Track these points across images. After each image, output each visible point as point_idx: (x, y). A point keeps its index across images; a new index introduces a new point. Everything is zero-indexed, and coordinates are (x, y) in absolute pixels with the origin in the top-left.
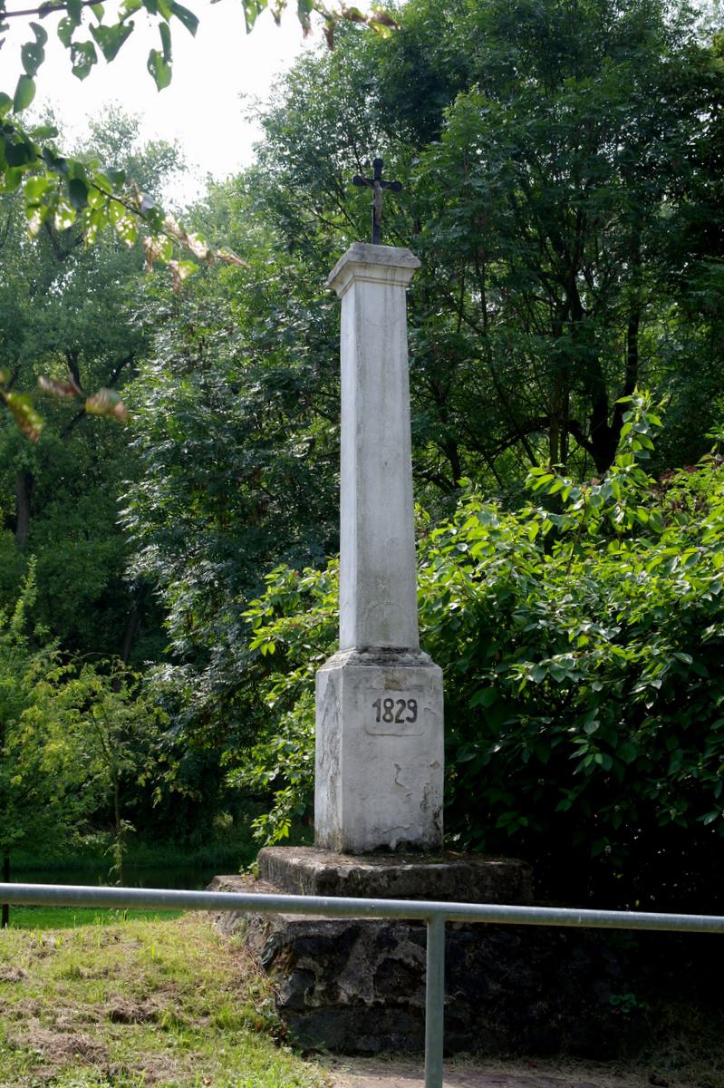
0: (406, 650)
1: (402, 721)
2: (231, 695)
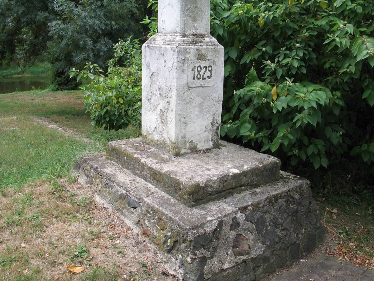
1: (205, 79)
2: (249, 231)
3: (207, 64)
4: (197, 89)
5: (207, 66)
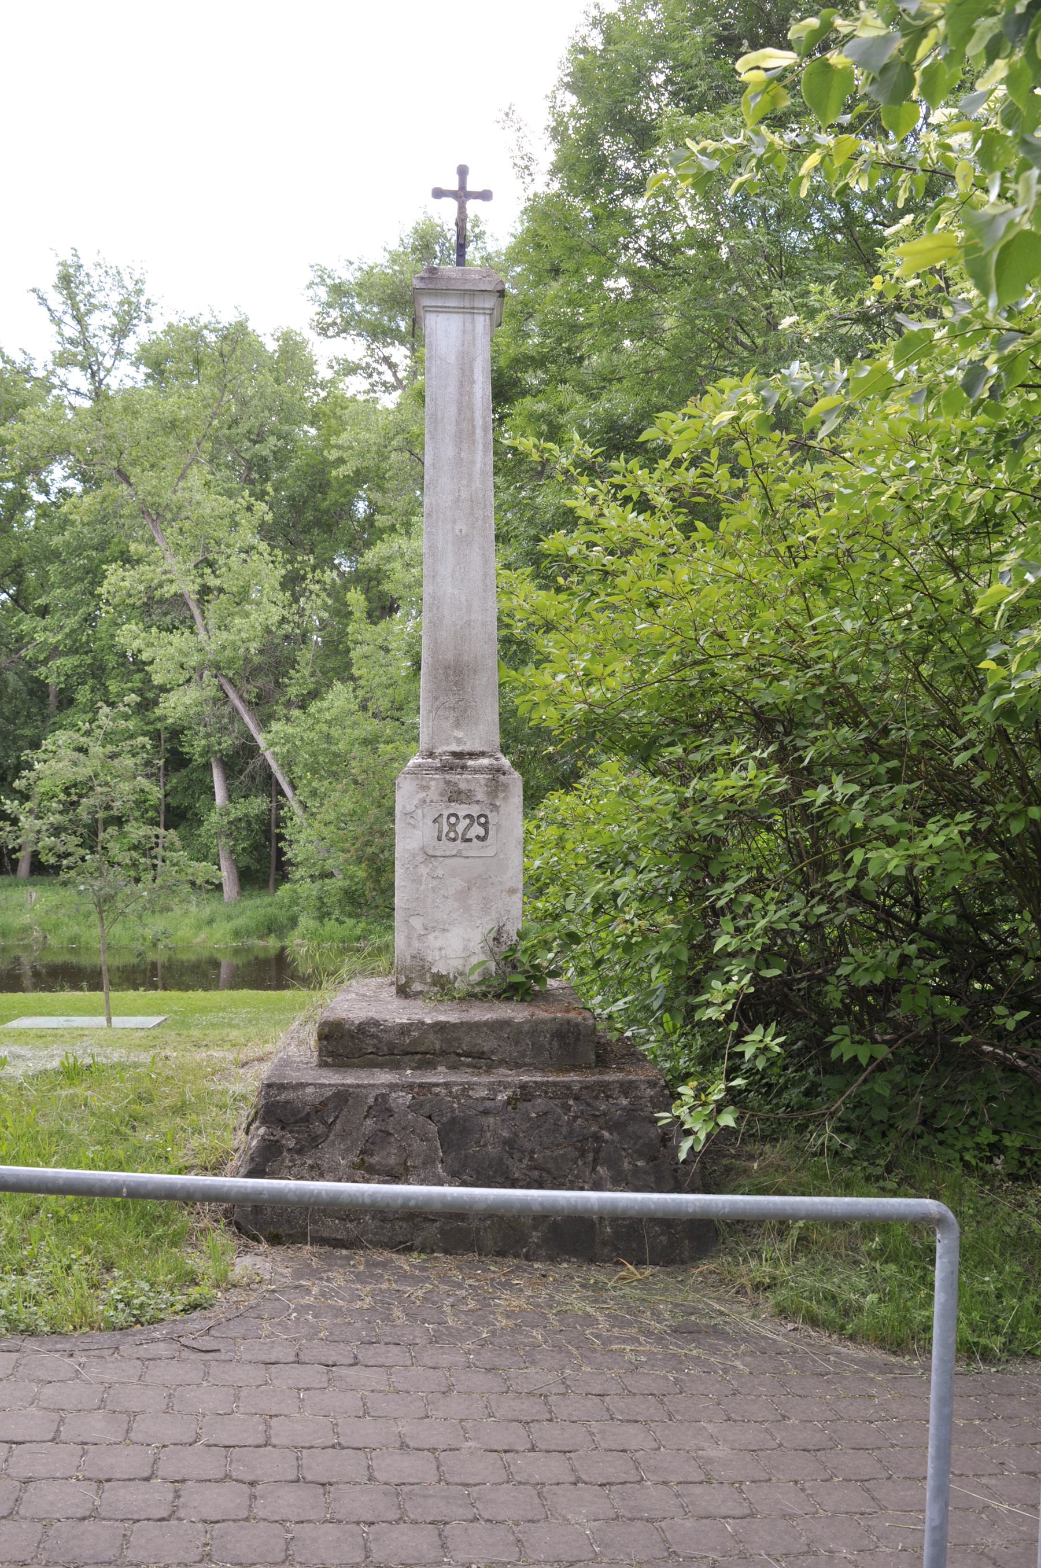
0: (483, 754)
1: (470, 840)
3: (475, 810)
4: (448, 861)
5: (475, 815)
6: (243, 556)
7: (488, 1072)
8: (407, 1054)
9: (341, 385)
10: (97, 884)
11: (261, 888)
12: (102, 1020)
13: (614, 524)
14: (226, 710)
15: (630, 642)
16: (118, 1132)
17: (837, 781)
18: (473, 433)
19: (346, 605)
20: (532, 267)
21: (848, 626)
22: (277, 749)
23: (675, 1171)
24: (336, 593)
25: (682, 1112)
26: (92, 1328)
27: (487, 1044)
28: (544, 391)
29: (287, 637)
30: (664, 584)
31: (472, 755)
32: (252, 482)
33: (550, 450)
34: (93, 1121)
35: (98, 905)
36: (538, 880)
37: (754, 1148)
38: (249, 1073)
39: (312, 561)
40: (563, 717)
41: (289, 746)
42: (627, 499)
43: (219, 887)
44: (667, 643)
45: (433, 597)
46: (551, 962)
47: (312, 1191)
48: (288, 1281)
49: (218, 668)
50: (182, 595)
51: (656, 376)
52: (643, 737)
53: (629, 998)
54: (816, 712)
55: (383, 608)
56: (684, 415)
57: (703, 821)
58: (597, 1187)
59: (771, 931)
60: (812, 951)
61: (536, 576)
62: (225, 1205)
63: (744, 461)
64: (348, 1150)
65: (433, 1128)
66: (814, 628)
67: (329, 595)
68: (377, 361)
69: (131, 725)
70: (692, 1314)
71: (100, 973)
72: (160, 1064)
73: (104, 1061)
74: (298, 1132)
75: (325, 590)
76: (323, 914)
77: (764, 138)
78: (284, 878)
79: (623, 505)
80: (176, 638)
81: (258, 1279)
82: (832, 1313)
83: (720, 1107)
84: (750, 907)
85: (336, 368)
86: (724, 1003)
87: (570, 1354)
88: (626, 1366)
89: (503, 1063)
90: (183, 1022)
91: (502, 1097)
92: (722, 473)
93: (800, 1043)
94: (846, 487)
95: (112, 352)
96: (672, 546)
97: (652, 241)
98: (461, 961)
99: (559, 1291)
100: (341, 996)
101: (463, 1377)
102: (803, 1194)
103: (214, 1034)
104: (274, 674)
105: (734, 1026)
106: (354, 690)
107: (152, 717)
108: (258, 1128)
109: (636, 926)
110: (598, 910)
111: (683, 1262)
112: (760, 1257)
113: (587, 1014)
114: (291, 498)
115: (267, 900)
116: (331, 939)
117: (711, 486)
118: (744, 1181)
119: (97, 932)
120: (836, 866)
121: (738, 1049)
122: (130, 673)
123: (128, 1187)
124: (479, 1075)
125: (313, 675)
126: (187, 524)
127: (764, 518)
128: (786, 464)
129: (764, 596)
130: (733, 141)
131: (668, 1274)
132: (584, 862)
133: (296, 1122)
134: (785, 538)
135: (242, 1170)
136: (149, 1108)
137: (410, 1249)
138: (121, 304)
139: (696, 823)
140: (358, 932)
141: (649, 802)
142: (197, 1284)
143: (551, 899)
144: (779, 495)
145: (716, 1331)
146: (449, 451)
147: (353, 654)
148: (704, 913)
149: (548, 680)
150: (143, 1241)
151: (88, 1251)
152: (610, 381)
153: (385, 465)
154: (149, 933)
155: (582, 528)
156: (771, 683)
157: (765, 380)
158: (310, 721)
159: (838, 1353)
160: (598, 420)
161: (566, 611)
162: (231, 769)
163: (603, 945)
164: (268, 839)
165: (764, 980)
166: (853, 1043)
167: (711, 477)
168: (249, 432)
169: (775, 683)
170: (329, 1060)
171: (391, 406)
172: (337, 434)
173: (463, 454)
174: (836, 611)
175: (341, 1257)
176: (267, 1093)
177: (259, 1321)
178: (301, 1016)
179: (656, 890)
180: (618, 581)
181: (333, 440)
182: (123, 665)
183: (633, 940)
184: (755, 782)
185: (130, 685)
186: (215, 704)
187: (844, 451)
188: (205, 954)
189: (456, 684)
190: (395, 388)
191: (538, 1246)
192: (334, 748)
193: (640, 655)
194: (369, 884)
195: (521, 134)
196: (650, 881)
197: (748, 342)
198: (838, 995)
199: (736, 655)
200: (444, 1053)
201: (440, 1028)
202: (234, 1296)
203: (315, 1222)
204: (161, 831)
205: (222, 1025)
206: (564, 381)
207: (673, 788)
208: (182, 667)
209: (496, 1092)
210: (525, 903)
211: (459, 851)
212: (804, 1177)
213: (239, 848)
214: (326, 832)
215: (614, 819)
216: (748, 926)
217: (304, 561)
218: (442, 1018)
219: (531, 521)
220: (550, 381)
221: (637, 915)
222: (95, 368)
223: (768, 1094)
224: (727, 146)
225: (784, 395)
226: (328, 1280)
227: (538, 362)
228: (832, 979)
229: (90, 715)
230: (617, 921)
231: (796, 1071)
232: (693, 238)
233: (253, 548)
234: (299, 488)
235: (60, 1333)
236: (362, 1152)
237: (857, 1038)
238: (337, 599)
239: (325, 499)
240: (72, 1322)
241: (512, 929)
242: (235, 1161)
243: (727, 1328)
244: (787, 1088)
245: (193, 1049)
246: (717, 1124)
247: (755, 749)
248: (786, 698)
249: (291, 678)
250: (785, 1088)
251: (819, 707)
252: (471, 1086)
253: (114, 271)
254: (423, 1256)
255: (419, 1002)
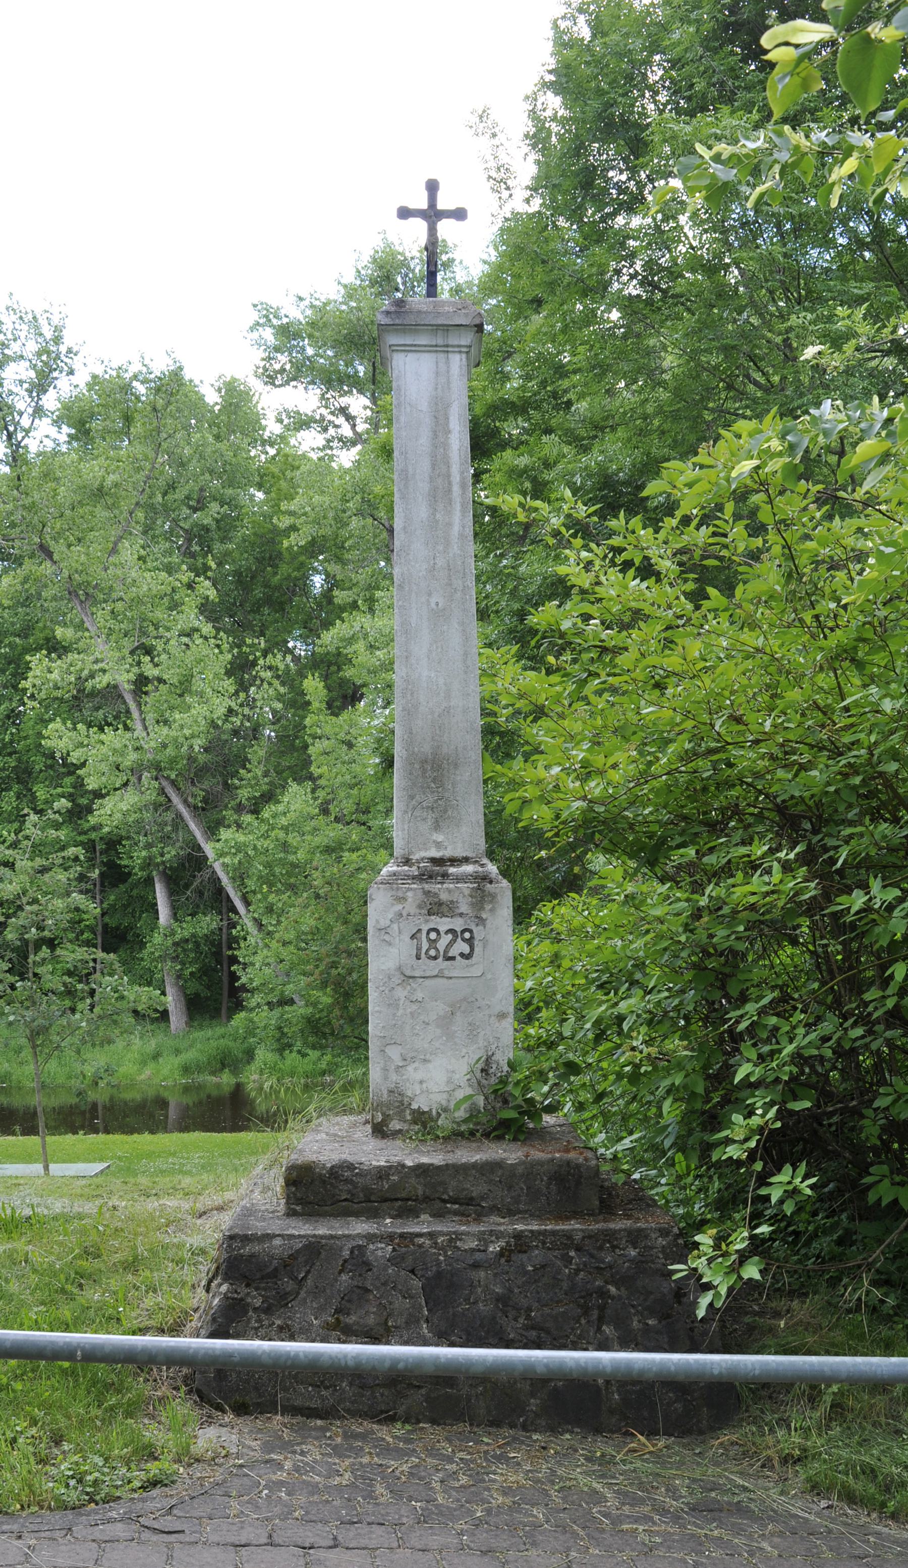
0: (466, 860)
1: (453, 958)
3: (458, 924)
4: (428, 982)
5: (459, 929)
6: (185, 640)
7: (477, 1220)
8: (386, 1200)
9: (293, 442)
10: (29, 1014)
11: (212, 1018)
12: (38, 1168)
13: (613, 593)
14: (169, 816)
15: (633, 728)
16: (63, 1291)
17: (875, 885)
18: (449, 491)
19: (303, 694)
20: (511, 297)
21: (887, 705)
22: (227, 860)
23: (692, 1330)
24: (291, 680)
25: (700, 1264)
26: (42, 1508)
27: (477, 1189)
28: (526, 443)
29: (236, 732)
30: (673, 661)
31: (454, 861)
32: (193, 555)
33: (536, 510)
34: (34, 1279)
35: (32, 1038)
36: (529, 1003)
37: (781, 1304)
38: (207, 1224)
39: (263, 645)
40: (557, 817)
41: (240, 856)
42: (627, 565)
43: (164, 1015)
44: (677, 729)
45: (407, 681)
46: (546, 1096)
47: (288, 1353)
48: (257, 1455)
49: (159, 769)
50: (116, 687)
51: (656, 422)
52: (650, 838)
53: (636, 1136)
54: (850, 806)
55: (345, 697)
56: (695, 465)
57: (721, 933)
58: (603, 1346)
59: (798, 1058)
60: (844, 1080)
61: (520, 656)
62: (185, 1370)
63: (765, 516)
64: (322, 1309)
65: (416, 1284)
66: (846, 709)
67: (283, 684)
68: (332, 413)
69: (62, 834)
70: (712, 1490)
71: (35, 1113)
72: (108, 1215)
73: (46, 1212)
74: (265, 1289)
75: (278, 677)
76: (283, 1046)
77: (787, 140)
78: (238, 1006)
79: (623, 571)
80: (109, 736)
81: (224, 1453)
82: (872, 1489)
83: (743, 1257)
84: (776, 1029)
85: (286, 421)
86: (746, 1140)
87: (575, 1535)
88: (639, 1547)
89: (494, 1209)
90: (128, 1169)
91: (494, 1248)
92: (738, 531)
93: (831, 1186)
94: (887, 545)
95: (30, 410)
96: (680, 617)
97: (650, 265)
98: (445, 1096)
99: (561, 1465)
100: (309, 1137)
101: (456, 1561)
102: (837, 1354)
103: (164, 1182)
104: (221, 774)
105: (758, 1166)
106: (313, 791)
107: (86, 826)
108: (220, 1285)
109: (644, 1054)
110: (600, 1037)
111: (701, 1432)
112: (789, 1427)
113: (590, 1154)
114: (237, 573)
115: (220, 1030)
116: (292, 1074)
117: (726, 547)
118: (769, 1341)
119: (30, 1068)
120: (872, 984)
121: (763, 1191)
122: (61, 776)
123: (83, 1350)
124: (467, 1223)
125: (266, 774)
126: (119, 605)
127: (788, 582)
128: (812, 519)
129: (788, 673)
130: (751, 145)
131: (684, 1446)
132: (583, 981)
133: (263, 1278)
134: (813, 606)
135: (203, 1332)
136: (97, 1264)
137: (391, 1420)
138: (39, 354)
139: (711, 936)
140: (323, 1065)
141: (658, 912)
142: (156, 1459)
143: (545, 1025)
144: (806, 556)
145: (739, 1509)
146: (422, 511)
147: (311, 750)
148: (721, 1041)
149: (542, 773)
150: (95, 1412)
151: (34, 1422)
152: (602, 429)
153: (344, 533)
154: (89, 1070)
155: (576, 598)
156: (796, 775)
157: (790, 423)
158: (264, 828)
159: (878, 1534)
160: (590, 476)
161: (560, 694)
162: (176, 883)
163: (605, 1077)
164: (219, 962)
165: (792, 1113)
166: (893, 1184)
167: (725, 536)
168: (188, 498)
169: (803, 774)
170: (298, 1208)
171: (348, 465)
172: (290, 498)
173: (438, 516)
174: (873, 689)
175: (316, 1428)
176: (229, 1246)
177: (227, 1499)
178: (265, 1160)
179: (666, 1013)
180: (619, 660)
181: (284, 506)
182: (51, 767)
183: (643, 1070)
184: (781, 887)
185: (59, 790)
186: (156, 810)
187: (879, 504)
188: (151, 1093)
189: (434, 780)
190: (354, 443)
191: (537, 1415)
192: (291, 858)
193: (645, 744)
194: (337, 1012)
195: (496, 141)
196: (659, 1002)
197: (762, 380)
198: (876, 1131)
199: (757, 742)
200: (427, 1199)
201: (422, 1170)
202: (198, 1471)
203: (285, 1389)
204: (100, 955)
205: (171, 1172)
206: (548, 431)
207: (686, 895)
208: (118, 768)
209: (487, 1243)
210: (516, 1030)
211: (441, 971)
212: (838, 1336)
213: (187, 972)
214: (285, 953)
215: (617, 934)
216: (772, 1053)
217: (252, 645)
218: (425, 1160)
219: (514, 593)
220: (534, 430)
221: (645, 1042)
222: (11, 429)
223: (795, 1243)
224: (744, 151)
225: (814, 440)
226: (302, 1453)
227: (519, 408)
228: (869, 1112)
229: (16, 825)
230: (624, 1048)
231: (827, 1217)
232: (695, 263)
233: (197, 630)
234: (246, 562)
235: (6, 1513)
236: (338, 1311)
237: (898, 1179)
238: (292, 687)
239: (276, 574)
240: (19, 1501)
241: (502, 1058)
242: (195, 1322)
243: (752, 1506)
244: (817, 1236)
245: (142, 1198)
246: (740, 1277)
247: (779, 849)
248: (815, 791)
249: (241, 779)
250: (815, 1236)
251: (853, 799)
252: (459, 1236)
253: (30, 316)
254: (408, 1427)
255: (399, 1143)
